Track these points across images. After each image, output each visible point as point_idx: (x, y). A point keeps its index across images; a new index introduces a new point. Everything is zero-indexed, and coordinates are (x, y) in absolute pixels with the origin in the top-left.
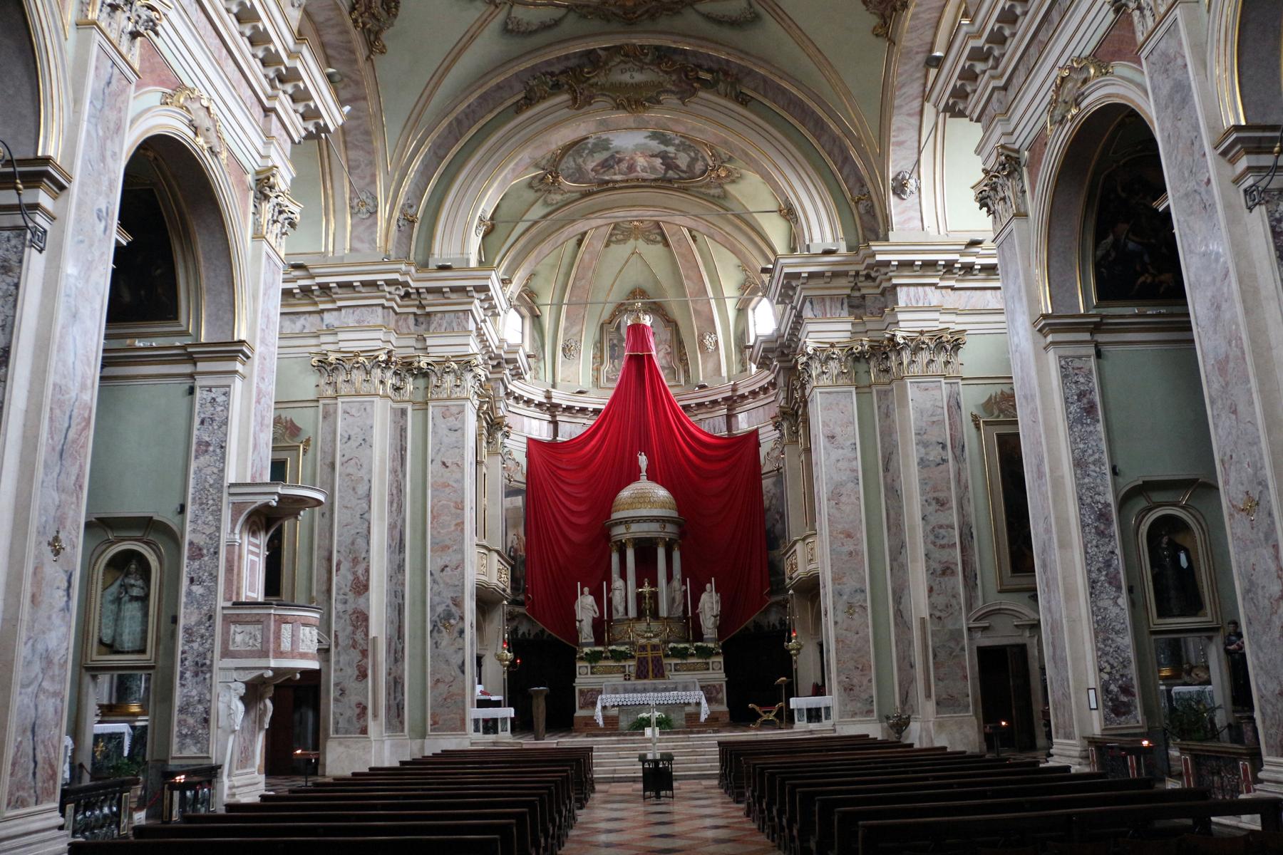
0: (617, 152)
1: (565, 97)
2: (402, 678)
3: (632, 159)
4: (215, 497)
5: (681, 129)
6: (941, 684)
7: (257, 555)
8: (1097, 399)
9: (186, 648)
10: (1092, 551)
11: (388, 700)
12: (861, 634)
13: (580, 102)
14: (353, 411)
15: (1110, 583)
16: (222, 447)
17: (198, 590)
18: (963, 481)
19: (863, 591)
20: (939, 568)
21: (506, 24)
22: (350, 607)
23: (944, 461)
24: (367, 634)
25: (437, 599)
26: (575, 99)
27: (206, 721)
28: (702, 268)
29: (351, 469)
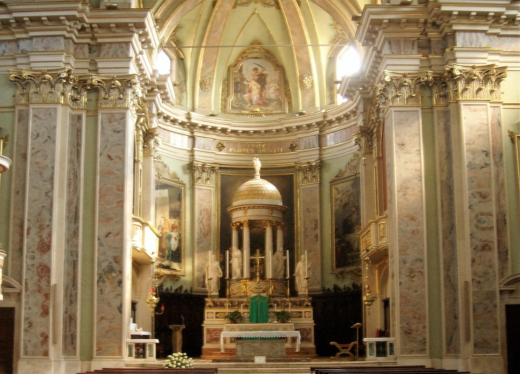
2: (75, 315)
14: (41, 115)
19: (421, 260)
20: (480, 244)
22: (36, 262)
24: (49, 282)
25: (102, 258)
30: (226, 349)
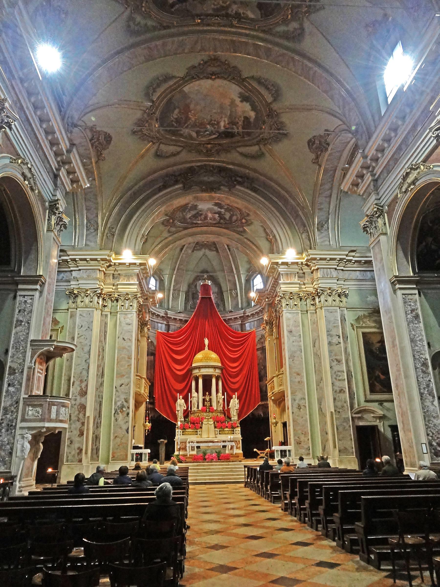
0: (200, 211)
1: (180, 186)
2: (99, 435)
3: (206, 214)
4: (24, 345)
5: (228, 202)
6: (340, 442)
7: (41, 374)
8: (420, 313)
9: (4, 417)
10: (421, 380)
11: (92, 446)
12: (304, 418)
13: (187, 188)
14: (84, 315)
15: (429, 395)
16: (28, 323)
17: (11, 389)
18: (347, 353)
19: (304, 399)
20: (338, 389)
21: (157, 152)
22: (78, 402)
23: (339, 343)
24: (85, 415)
25: (118, 399)
26: (184, 187)
27: (11, 454)
28: (232, 262)
29: (82, 340)
30: (190, 455)
